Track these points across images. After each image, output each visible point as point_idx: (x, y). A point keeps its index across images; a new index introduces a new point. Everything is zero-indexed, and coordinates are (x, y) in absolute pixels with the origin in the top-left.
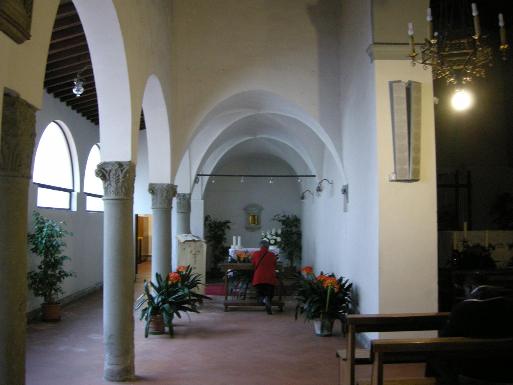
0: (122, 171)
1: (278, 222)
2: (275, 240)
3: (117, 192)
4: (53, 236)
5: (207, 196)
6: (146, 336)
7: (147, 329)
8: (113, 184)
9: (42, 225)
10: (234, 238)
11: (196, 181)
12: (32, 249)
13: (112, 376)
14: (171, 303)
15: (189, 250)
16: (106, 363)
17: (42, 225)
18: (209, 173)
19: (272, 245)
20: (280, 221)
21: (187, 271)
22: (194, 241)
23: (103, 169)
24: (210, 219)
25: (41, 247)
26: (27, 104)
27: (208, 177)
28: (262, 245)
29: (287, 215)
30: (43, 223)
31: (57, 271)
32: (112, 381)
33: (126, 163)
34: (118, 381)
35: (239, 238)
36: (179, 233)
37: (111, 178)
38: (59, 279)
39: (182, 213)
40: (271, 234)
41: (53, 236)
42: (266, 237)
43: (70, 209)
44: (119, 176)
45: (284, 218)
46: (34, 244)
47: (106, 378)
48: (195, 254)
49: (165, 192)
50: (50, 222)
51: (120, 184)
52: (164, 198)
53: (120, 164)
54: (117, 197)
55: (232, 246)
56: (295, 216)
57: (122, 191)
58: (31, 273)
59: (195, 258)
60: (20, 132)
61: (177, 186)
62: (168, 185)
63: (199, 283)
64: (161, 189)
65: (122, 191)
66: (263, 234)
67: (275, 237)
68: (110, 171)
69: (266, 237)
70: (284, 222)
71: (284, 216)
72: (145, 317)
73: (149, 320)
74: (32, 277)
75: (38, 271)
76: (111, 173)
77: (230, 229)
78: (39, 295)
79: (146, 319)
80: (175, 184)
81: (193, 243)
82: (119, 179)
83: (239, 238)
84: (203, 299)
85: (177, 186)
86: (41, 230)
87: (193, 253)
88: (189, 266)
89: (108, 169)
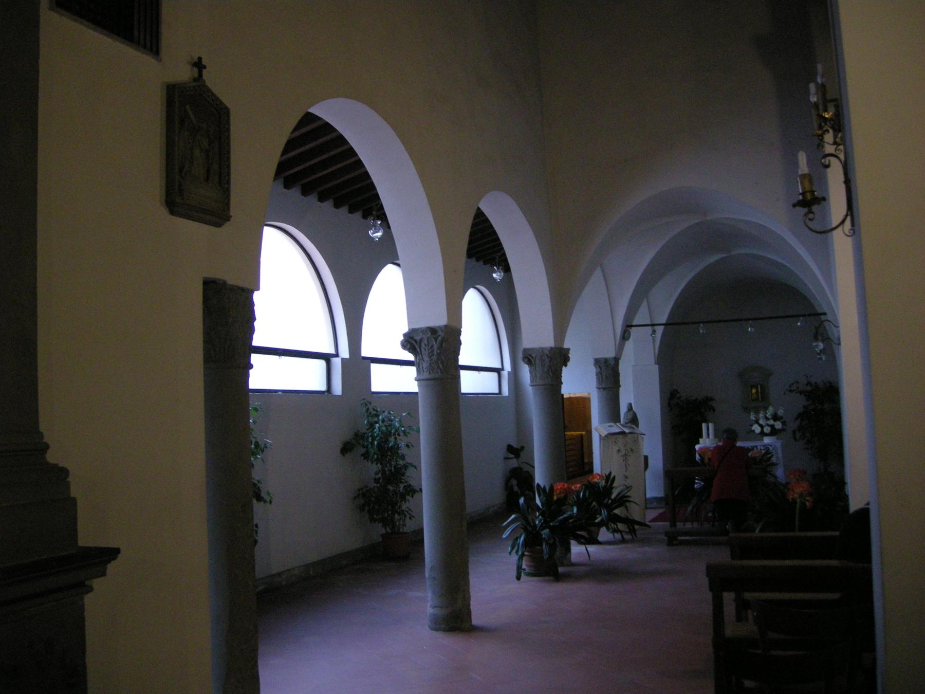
0: (436, 340)
1: (798, 394)
2: (772, 426)
3: (431, 369)
4: (390, 434)
5: (667, 358)
6: (518, 578)
7: (519, 568)
8: (426, 358)
9: (376, 419)
10: (704, 425)
11: (625, 336)
12: (362, 455)
13: (435, 623)
14: (552, 529)
15: (616, 448)
16: (429, 604)
17: (376, 419)
18: (664, 322)
19: (766, 435)
20: (801, 393)
21: (607, 482)
22: (623, 433)
23: (412, 338)
24: (678, 395)
25: (372, 451)
26: (239, 288)
27: (662, 327)
28: (725, 436)
29: (813, 380)
30: (377, 416)
31: (402, 486)
32: (437, 630)
33: (440, 327)
34: (444, 630)
35: (711, 425)
36: (601, 422)
37: (423, 350)
38: (403, 497)
39: (604, 389)
40: (767, 419)
41: (390, 434)
42: (757, 422)
43: (500, 392)
44: (432, 346)
45: (809, 388)
46: (364, 447)
47: (430, 627)
48: (626, 455)
49: (547, 360)
50: (386, 413)
51: (435, 358)
52: (546, 370)
53: (433, 331)
54: (430, 377)
55: (701, 440)
56: (830, 383)
57: (438, 367)
58: (362, 489)
59: (625, 460)
60: (230, 320)
61: (569, 350)
62: (552, 348)
63: (629, 501)
64: (541, 356)
65: (438, 367)
66: (753, 417)
67: (771, 422)
68: (421, 340)
69: (757, 422)
70: (809, 395)
71: (809, 383)
72: (514, 551)
73: (520, 553)
74: (364, 495)
75: (372, 485)
76: (423, 344)
77: (714, 410)
78: (375, 520)
79: (517, 552)
80: (565, 346)
81: (621, 436)
82: (433, 351)
83: (711, 425)
84: (636, 527)
85: (569, 350)
86: (372, 426)
87: (623, 453)
88: (610, 474)
89: (418, 338)
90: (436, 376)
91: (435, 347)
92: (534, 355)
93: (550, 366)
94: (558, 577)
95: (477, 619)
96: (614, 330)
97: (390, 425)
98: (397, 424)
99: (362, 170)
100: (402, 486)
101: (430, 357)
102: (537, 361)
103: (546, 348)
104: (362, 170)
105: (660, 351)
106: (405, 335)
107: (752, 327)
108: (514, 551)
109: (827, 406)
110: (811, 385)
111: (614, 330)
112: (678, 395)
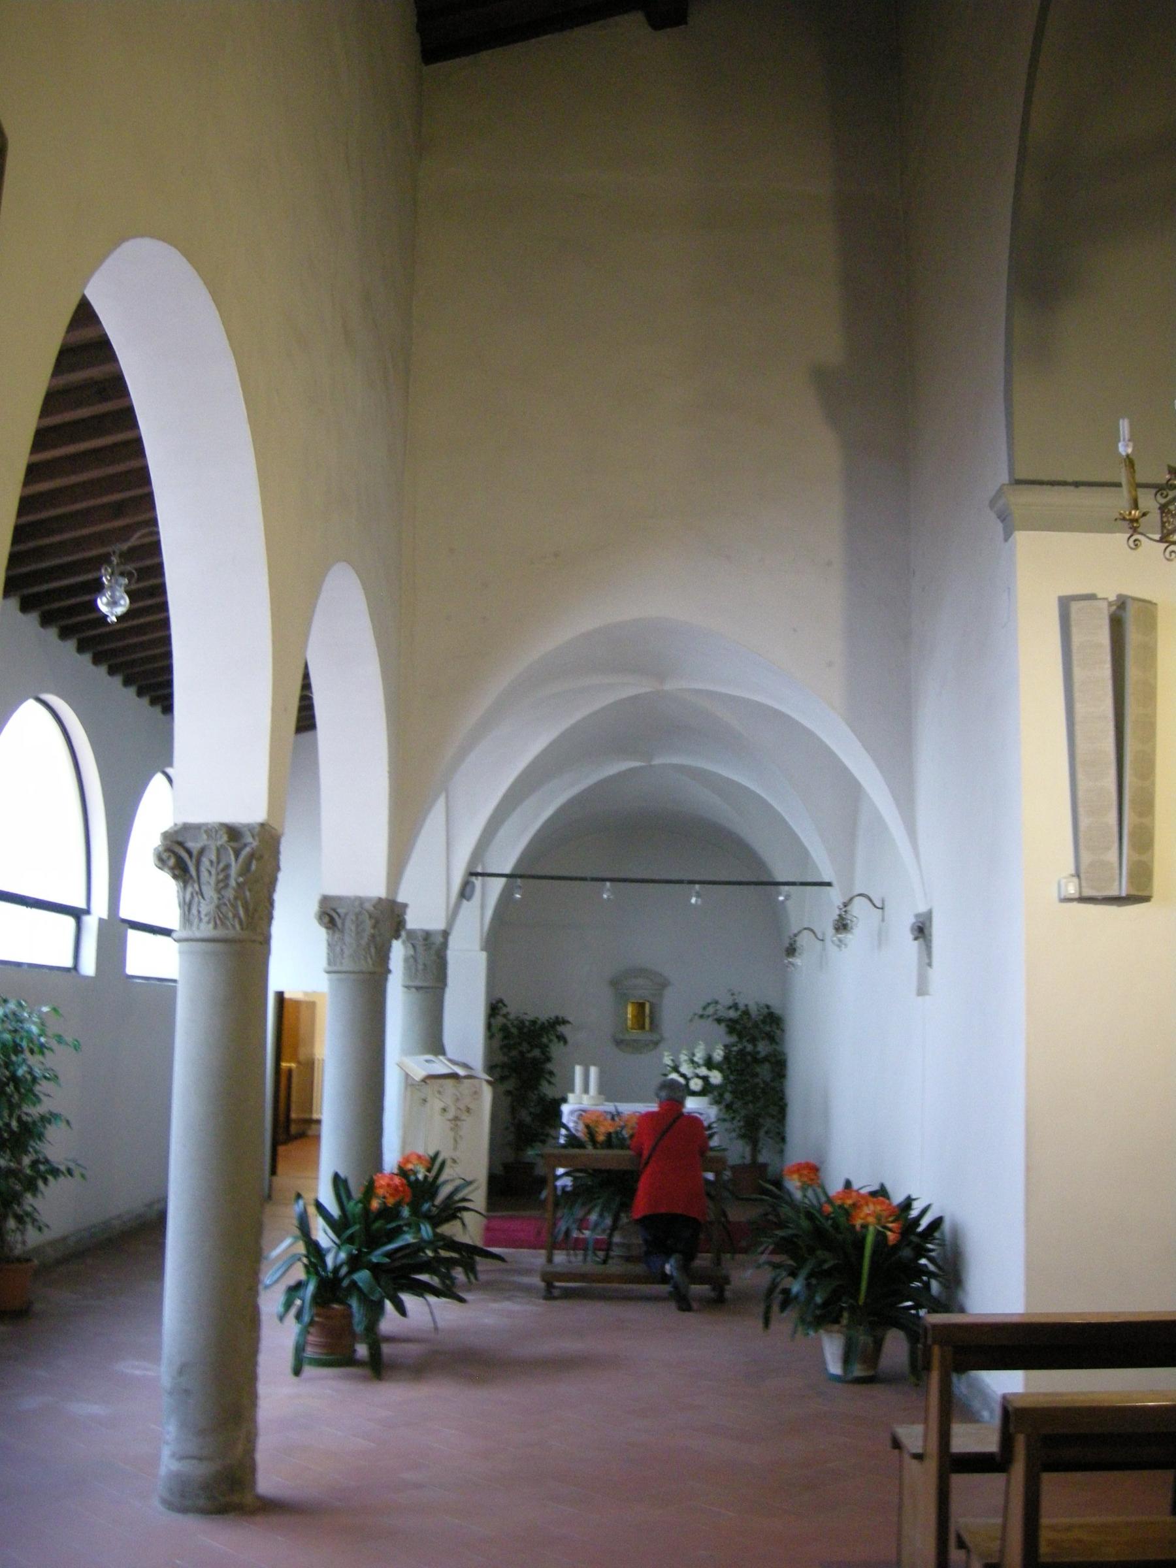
0: (237, 854)
2: (705, 1079)
3: (219, 919)
5: (497, 940)
6: (297, 1371)
7: (299, 1349)
8: (209, 892)
14: (375, 1269)
15: (438, 1105)
16: (166, 1452)
18: (507, 871)
19: (694, 1094)
20: (719, 1021)
22: (454, 1076)
23: (181, 844)
24: (504, 1011)
28: (663, 1094)
31: (26, 1161)
32: (184, 1510)
33: (250, 827)
34: (204, 1512)
35: (593, 1071)
37: (204, 875)
39: (418, 988)
44: (228, 867)
45: (732, 1014)
48: (456, 1119)
49: (369, 923)
51: (230, 893)
52: (364, 942)
53: (233, 833)
56: (768, 1007)
57: (236, 915)
61: (405, 906)
62: (380, 899)
65: (236, 915)
66: (667, 1060)
67: (703, 1071)
68: (202, 851)
70: (733, 1026)
71: (735, 1006)
72: (293, 1311)
76: (205, 861)
77: (565, 1042)
80: (401, 899)
81: (449, 1083)
82: (227, 877)
83: (593, 1071)
85: (405, 906)
87: (451, 1114)
88: (437, 1155)
89: (194, 846)
90: (230, 933)
91: (234, 871)
92: (341, 911)
93: (373, 936)
94: (377, 1368)
95: (268, 1482)
96: (448, 883)
97: (16, 1031)
98: (35, 1029)
99: (134, 464)
100: (26, 1161)
101: (218, 891)
102: (348, 923)
103: (369, 899)
104: (134, 464)
105: (490, 929)
106: (166, 836)
107: (698, 895)
108: (293, 1311)
109: (763, 1048)
110: (737, 1009)
111: (448, 883)
112: (504, 1011)
